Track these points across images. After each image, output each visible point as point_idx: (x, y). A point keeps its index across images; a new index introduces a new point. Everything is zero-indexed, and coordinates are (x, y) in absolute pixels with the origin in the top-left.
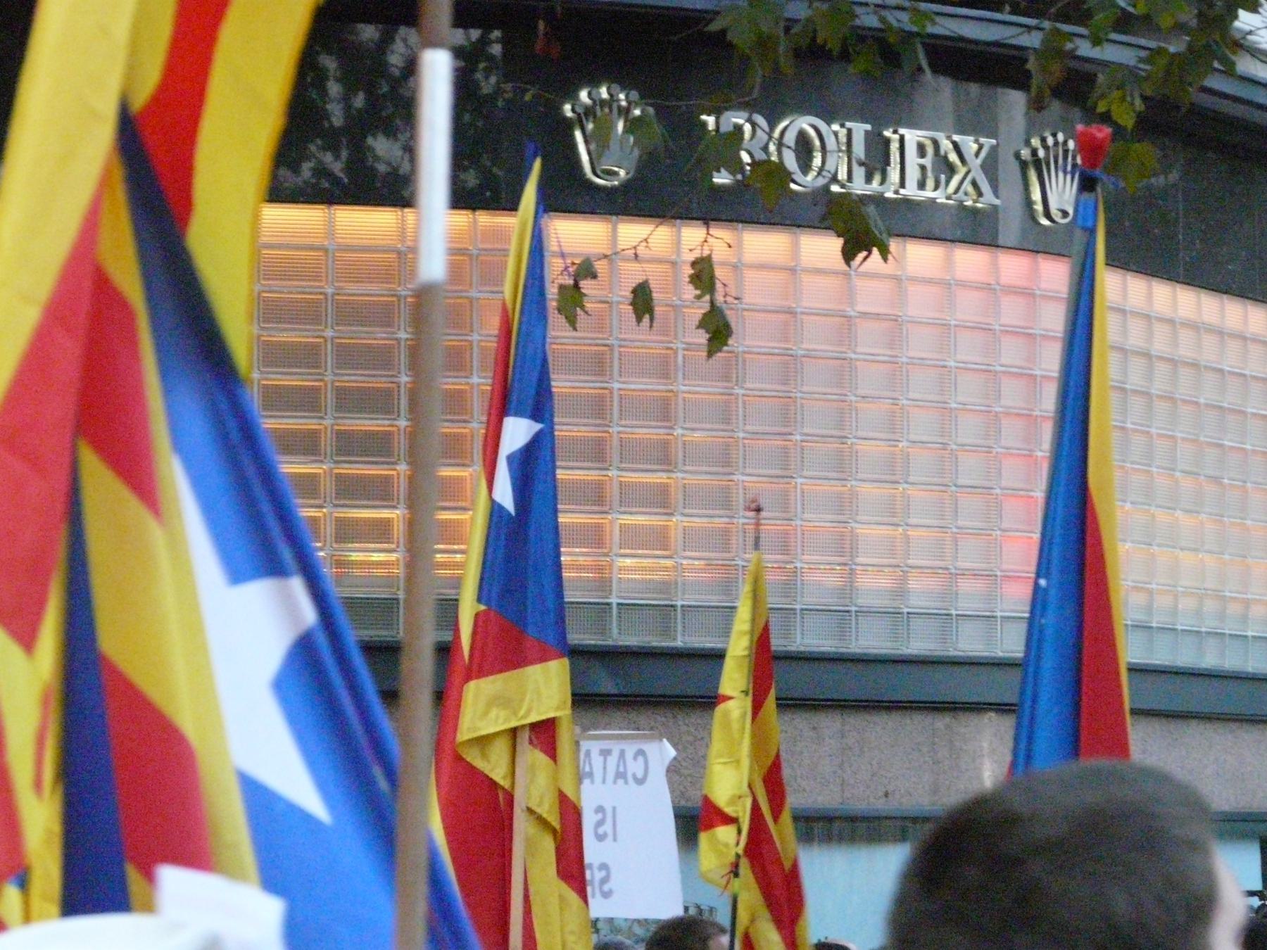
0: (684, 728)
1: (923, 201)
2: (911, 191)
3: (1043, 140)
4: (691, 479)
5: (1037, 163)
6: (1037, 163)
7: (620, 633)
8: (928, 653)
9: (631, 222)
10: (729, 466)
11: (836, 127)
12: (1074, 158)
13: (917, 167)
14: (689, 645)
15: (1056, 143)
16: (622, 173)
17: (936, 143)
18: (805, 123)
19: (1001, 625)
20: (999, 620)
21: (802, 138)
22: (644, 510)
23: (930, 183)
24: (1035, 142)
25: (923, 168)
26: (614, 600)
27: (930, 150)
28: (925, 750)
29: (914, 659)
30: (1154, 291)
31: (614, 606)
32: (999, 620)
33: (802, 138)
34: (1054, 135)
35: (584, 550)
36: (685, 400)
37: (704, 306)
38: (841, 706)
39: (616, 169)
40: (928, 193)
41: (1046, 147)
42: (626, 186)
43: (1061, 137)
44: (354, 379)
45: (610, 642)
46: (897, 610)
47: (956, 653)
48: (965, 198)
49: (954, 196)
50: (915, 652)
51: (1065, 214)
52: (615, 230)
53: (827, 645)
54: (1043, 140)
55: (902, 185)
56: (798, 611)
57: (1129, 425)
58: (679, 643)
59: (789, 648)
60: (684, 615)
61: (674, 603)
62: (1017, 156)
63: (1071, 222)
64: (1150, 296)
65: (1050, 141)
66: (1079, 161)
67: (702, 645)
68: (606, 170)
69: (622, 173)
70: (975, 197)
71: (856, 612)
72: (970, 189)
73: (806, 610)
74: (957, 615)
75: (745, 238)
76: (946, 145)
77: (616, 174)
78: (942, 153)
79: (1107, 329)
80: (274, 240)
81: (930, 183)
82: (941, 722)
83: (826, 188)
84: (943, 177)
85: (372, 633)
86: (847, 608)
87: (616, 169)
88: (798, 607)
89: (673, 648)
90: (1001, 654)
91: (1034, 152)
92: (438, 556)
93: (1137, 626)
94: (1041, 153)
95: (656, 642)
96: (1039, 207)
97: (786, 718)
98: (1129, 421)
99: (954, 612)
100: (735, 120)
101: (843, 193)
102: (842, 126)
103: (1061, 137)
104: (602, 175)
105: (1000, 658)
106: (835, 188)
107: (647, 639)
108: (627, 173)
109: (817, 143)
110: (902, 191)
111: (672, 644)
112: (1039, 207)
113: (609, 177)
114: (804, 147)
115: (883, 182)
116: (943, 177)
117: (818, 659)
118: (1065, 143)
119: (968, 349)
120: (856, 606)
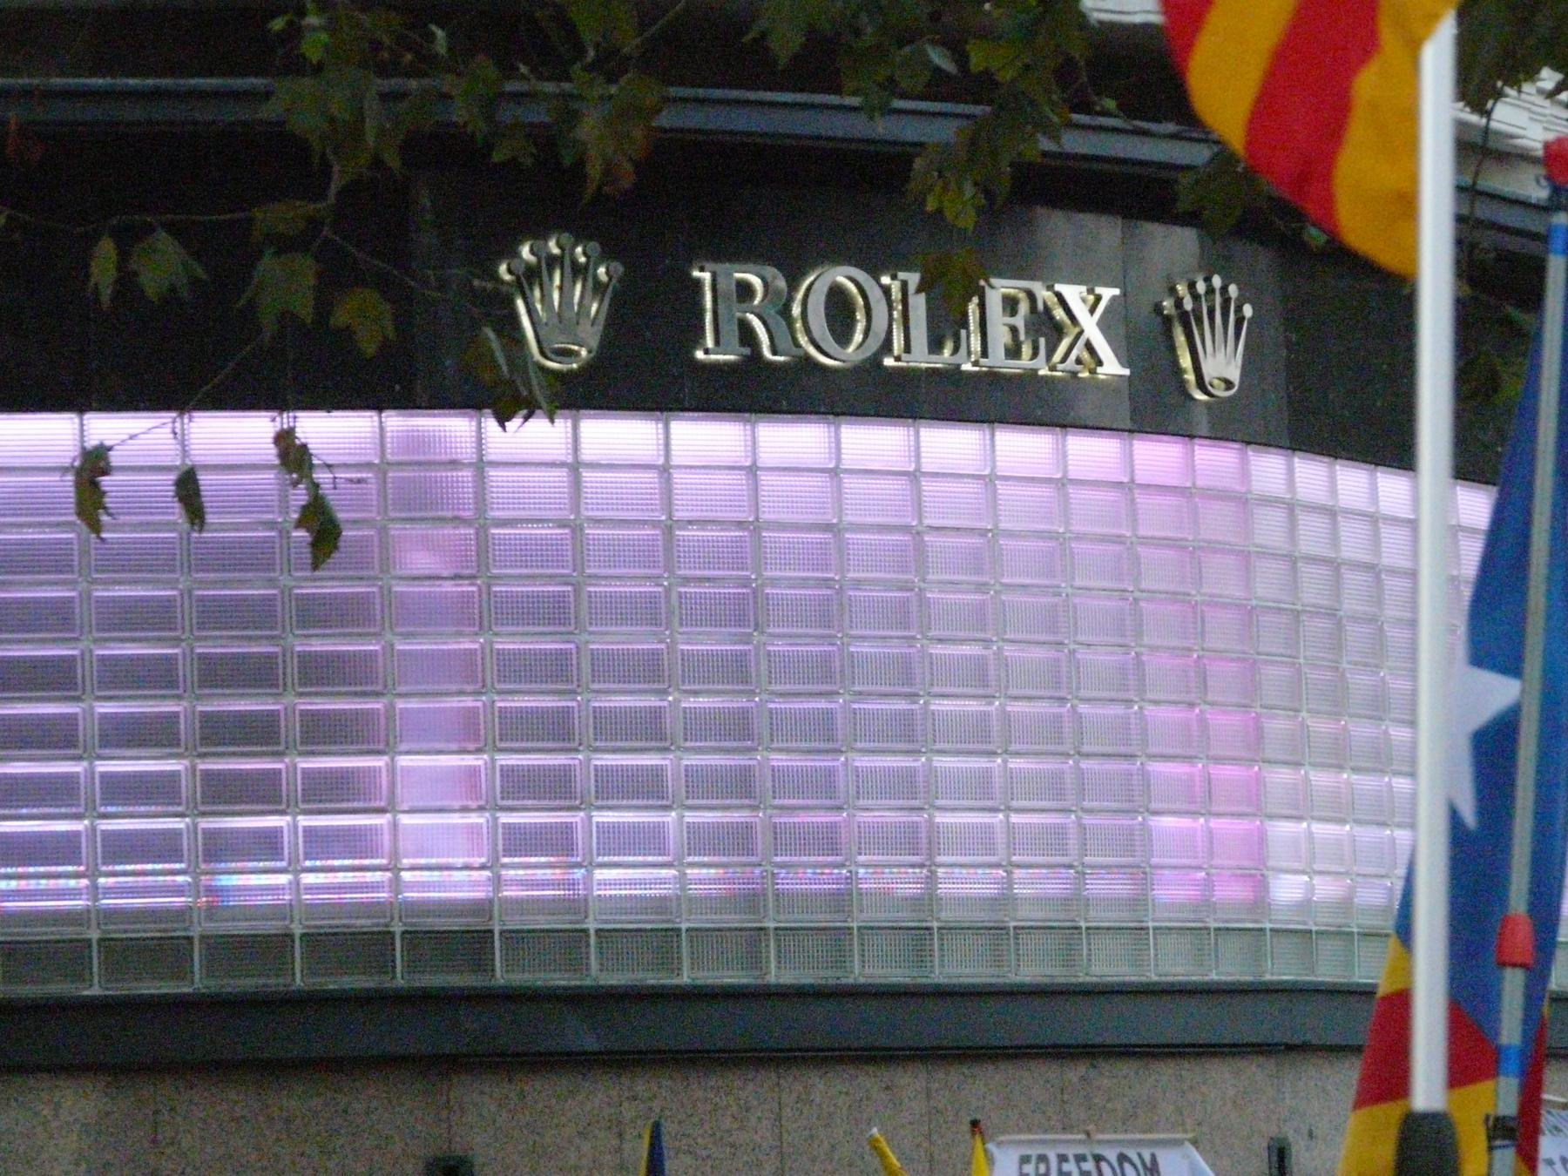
0: (700, 1094)
1: (1015, 375)
2: (998, 359)
3: (1192, 286)
4: (779, 760)
5: (1184, 318)
6: (1184, 318)
7: (601, 970)
8: (1046, 980)
9: (595, 417)
10: (595, 734)
11: (886, 280)
12: (1239, 309)
13: (1006, 329)
14: (699, 982)
15: (1210, 290)
16: (584, 353)
17: (1031, 296)
18: (842, 276)
19: (1155, 939)
20: (1151, 932)
21: (836, 294)
22: (710, 802)
23: (1026, 350)
24: (1182, 289)
25: (1014, 330)
26: (591, 926)
27: (1024, 308)
28: (1050, 1111)
29: (1214, 988)
30: (843, 435)
31: (592, 932)
32: (1151, 932)
33: (836, 294)
34: (1208, 280)
35: (552, 859)
36: (769, 655)
37: (300, 496)
38: (1088, 1053)
39: (576, 348)
40: (1025, 362)
41: (1196, 297)
42: (589, 370)
43: (1217, 281)
44: (218, 646)
45: (588, 982)
46: (1001, 925)
47: (1088, 979)
48: (1079, 367)
49: (1060, 367)
50: (1027, 980)
51: (1228, 384)
52: (575, 428)
53: (898, 975)
54: (1192, 286)
55: (985, 353)
56: (855, 931)
57: (1345, 665)
58: (685, 978)
59: (844, 981)
60: (691, 941)
61: (677, 926)
62: (1158, 309)
63: (1230, 399)
64: (1374, 489)
65: (1201, 287)
66: (1248, 311)
67: (718, 982)
68: (559, 349)
69: (584, 353)
70: (1093, 366)
71: (939, 928)
72: (1086, 356)
73: (865, 928)
74: (1088, 928)
75: (761, 433)
76: (1043, 294)
77: (577, 354)
78: (1040, 307)
79: (763, 492)
80: (784, 517)
81: (1026, 350)
82: (1074, 1073)
83: (875, 362)
84: (1042, 341)
85: (261, 981)
86: (924, 924)
87: (576, 348)
88: (855, 925)
89: (677, 986)
90: (1155, 978)
91: (1179, 303)
92: (203, 878)
93: (1366, 935)
94: (1188, 305)
95: (652, 979)
96: (1190, 377)
97: (845, 1076)
98: (1345, 659)
99: (1083, 924)
100: (738, 275)
101: (978, 372)
102: (894, 277)
103: (1217, 281)
104: (553, 356)
105: (1155, 984)
106: (889, 362)
107: (640, 975)
108: (590, 352)
109: (860, 301)
110: (983, 361)
111: (675, 981)
112: (1190, 377)
113: (566, 359)
114: (840, 310)
115: (956, 350)
116: (1042, 341)
117: (1277, 991)
118: (1224, 289)
119: (1159, 572)
120: (938, 919)
